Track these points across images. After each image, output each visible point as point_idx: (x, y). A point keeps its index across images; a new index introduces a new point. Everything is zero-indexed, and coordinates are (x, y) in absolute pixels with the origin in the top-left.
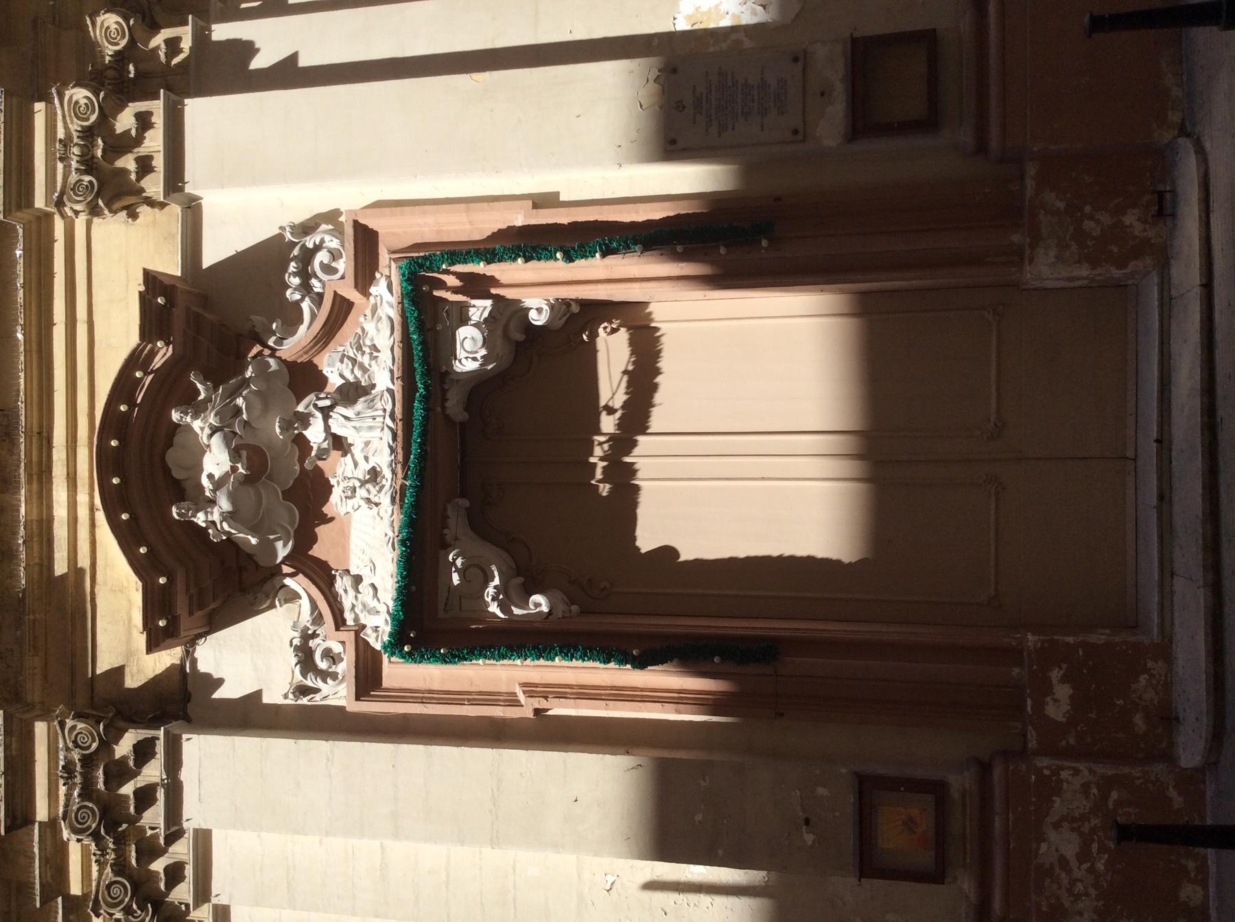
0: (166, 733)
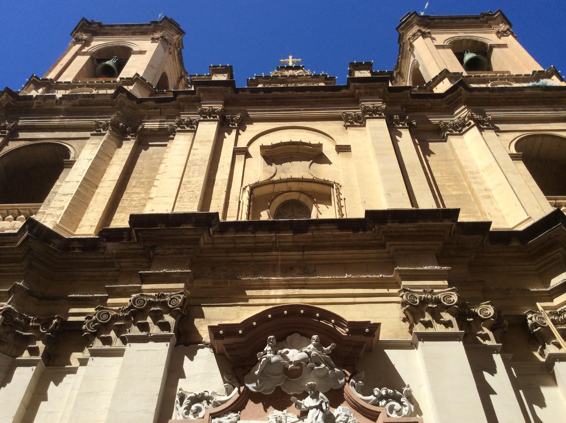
0: (171, 335)
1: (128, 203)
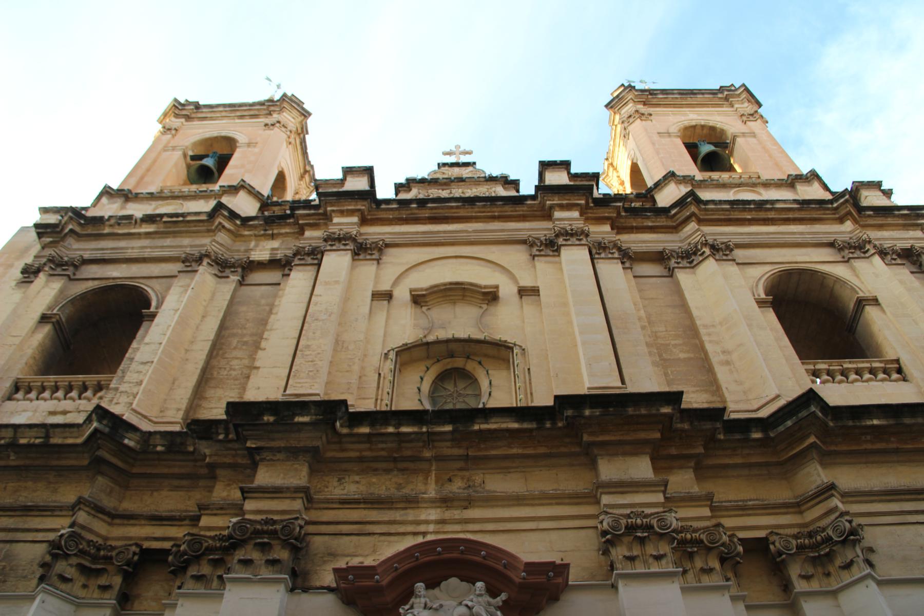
1: (225, 373)
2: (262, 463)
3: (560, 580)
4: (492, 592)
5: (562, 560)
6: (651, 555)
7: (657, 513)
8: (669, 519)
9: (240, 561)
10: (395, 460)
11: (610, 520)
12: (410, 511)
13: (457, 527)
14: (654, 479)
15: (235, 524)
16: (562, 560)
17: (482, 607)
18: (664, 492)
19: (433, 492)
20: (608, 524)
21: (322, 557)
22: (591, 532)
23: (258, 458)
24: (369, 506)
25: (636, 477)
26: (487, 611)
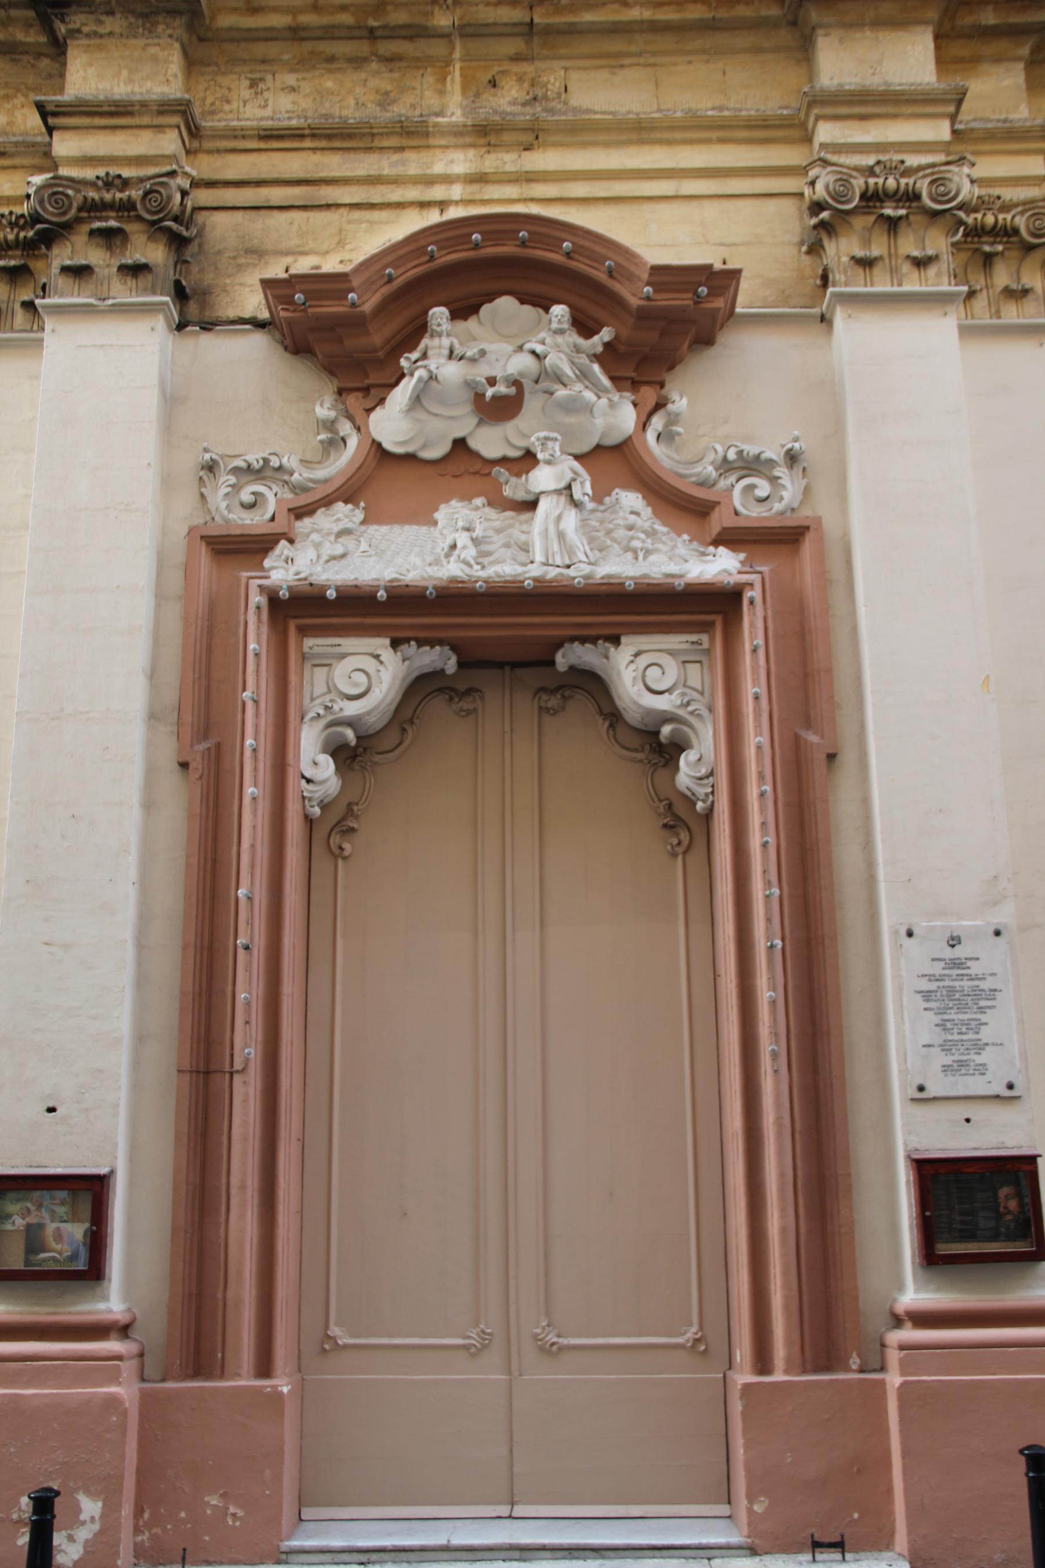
2: (76, 42)
3: (719, 303)
4: (585, 327)
5: (724, 263)
6: (908, 257)
7: (933, 165)
8: (956, 179)
9: (65, 270)
10: (372, 35)
11: (831, 178)
12: (410, 155)
13: (511, 191)
14: (936, 86)
15: (40, 189)
16: (724, 263)
17: (562, 356)
18: (953, 118)
19: (459, 112)
20: (827, 187)
21: (234, 258)
22: (788, 206)
23: (62, 29)
24: (323, 144)
25: (897, 80)
26: (573, 363)
